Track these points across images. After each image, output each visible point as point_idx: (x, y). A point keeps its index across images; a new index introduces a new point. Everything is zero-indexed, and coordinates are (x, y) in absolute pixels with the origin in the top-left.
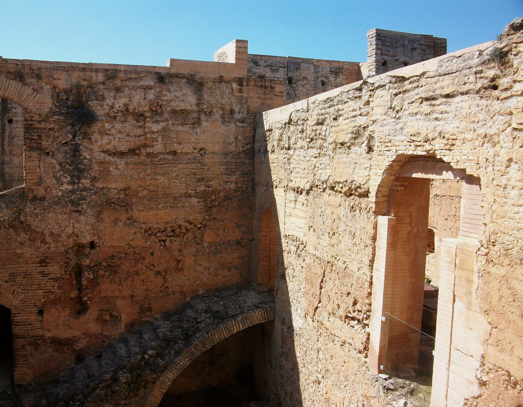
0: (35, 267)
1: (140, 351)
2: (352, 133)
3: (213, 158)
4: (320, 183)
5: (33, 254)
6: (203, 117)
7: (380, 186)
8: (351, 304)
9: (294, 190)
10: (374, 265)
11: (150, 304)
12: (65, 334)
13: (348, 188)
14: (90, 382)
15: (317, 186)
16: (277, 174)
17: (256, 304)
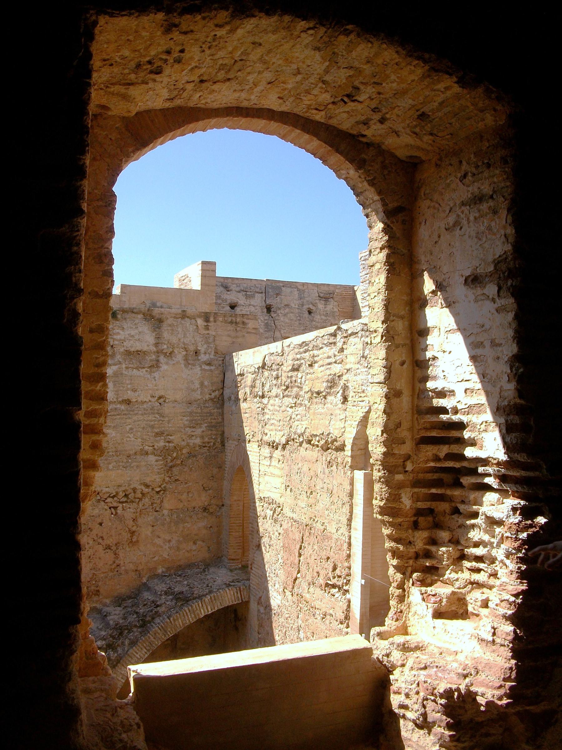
2: (328, 381)
3: (174, 407)
4: (296, 436)
6: (162, 359)
7: (355, 439)
8: (331, 570)
9: (269, 445)
10: (352, 524)
11: (97, 587)
13: (324, 441)
15: (293, 440)
16: (250, 427)
17: (228, 582)
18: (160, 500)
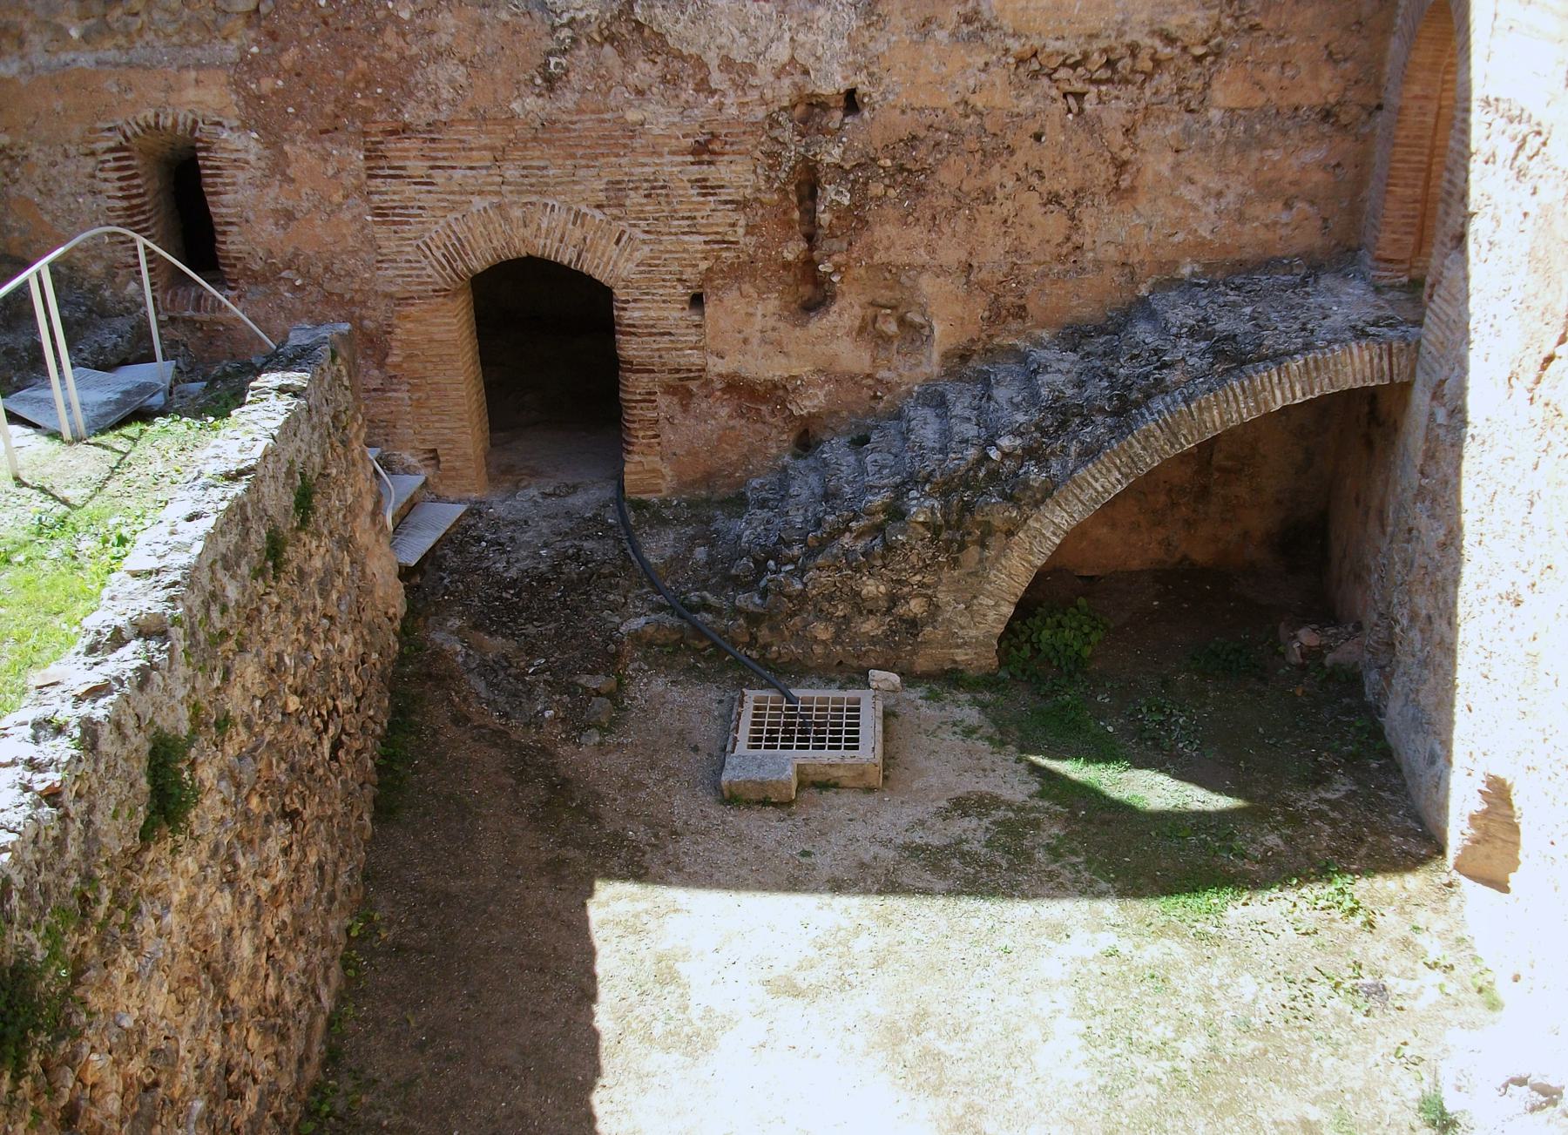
0: (678, 164)
1: (979, 437)
5: (674, 124)
12: (763, 367)
14: (826, 513)
17: (1361, 324)
18: (1201, 82)
